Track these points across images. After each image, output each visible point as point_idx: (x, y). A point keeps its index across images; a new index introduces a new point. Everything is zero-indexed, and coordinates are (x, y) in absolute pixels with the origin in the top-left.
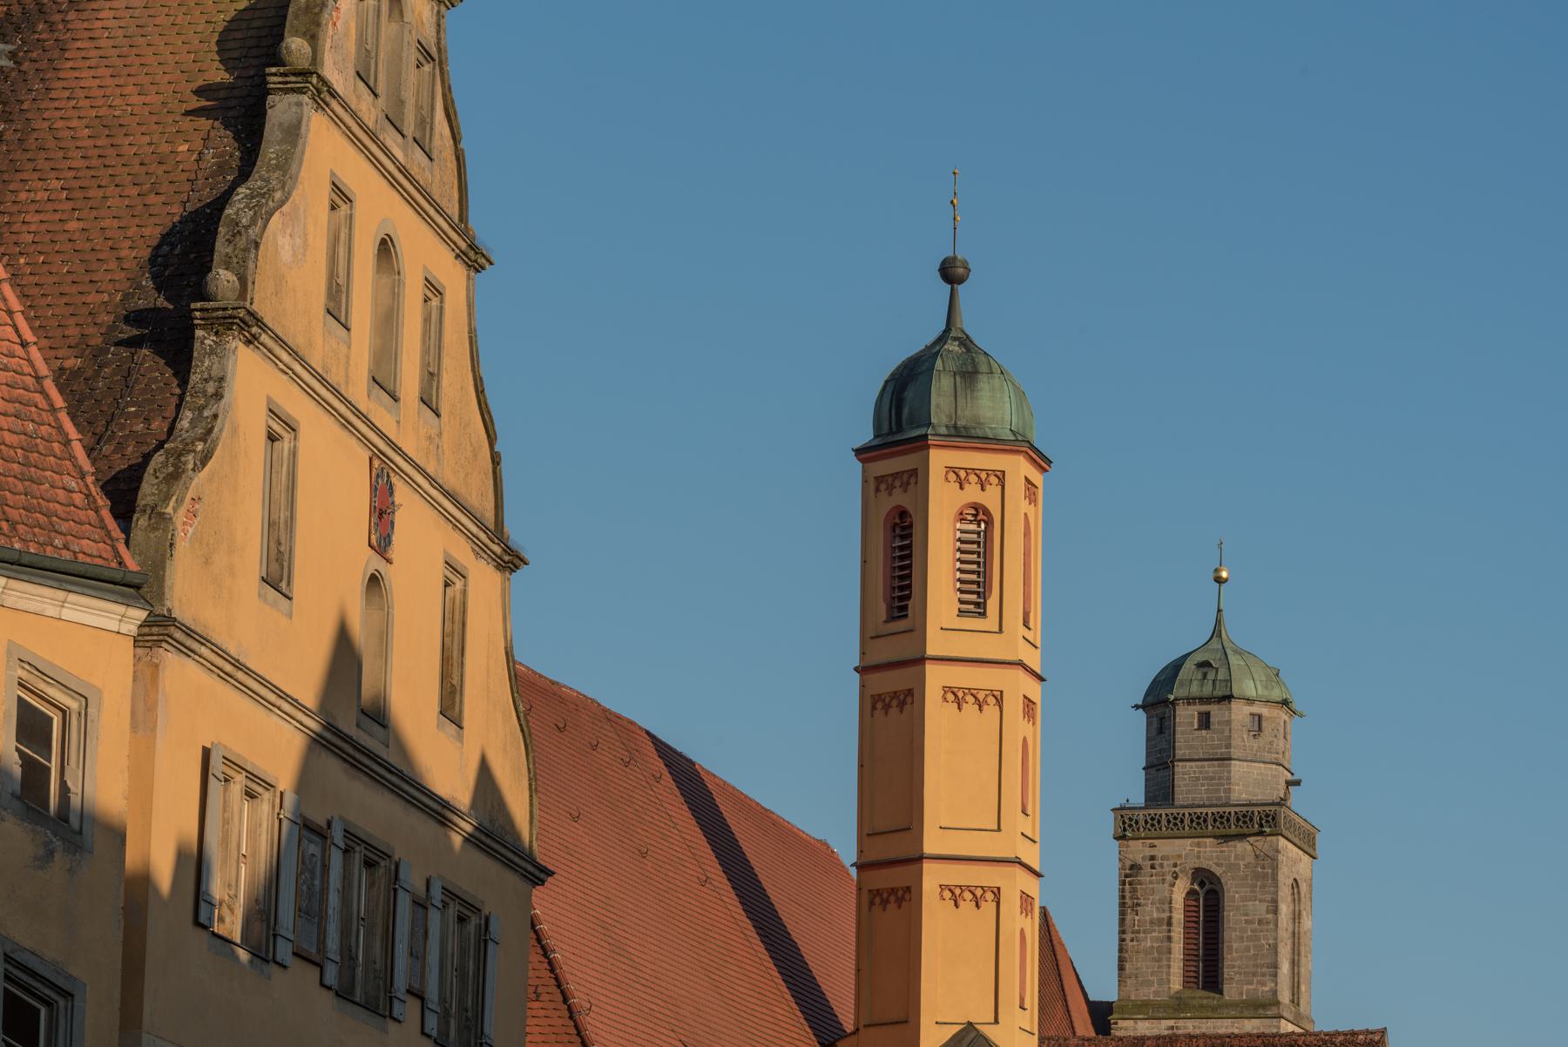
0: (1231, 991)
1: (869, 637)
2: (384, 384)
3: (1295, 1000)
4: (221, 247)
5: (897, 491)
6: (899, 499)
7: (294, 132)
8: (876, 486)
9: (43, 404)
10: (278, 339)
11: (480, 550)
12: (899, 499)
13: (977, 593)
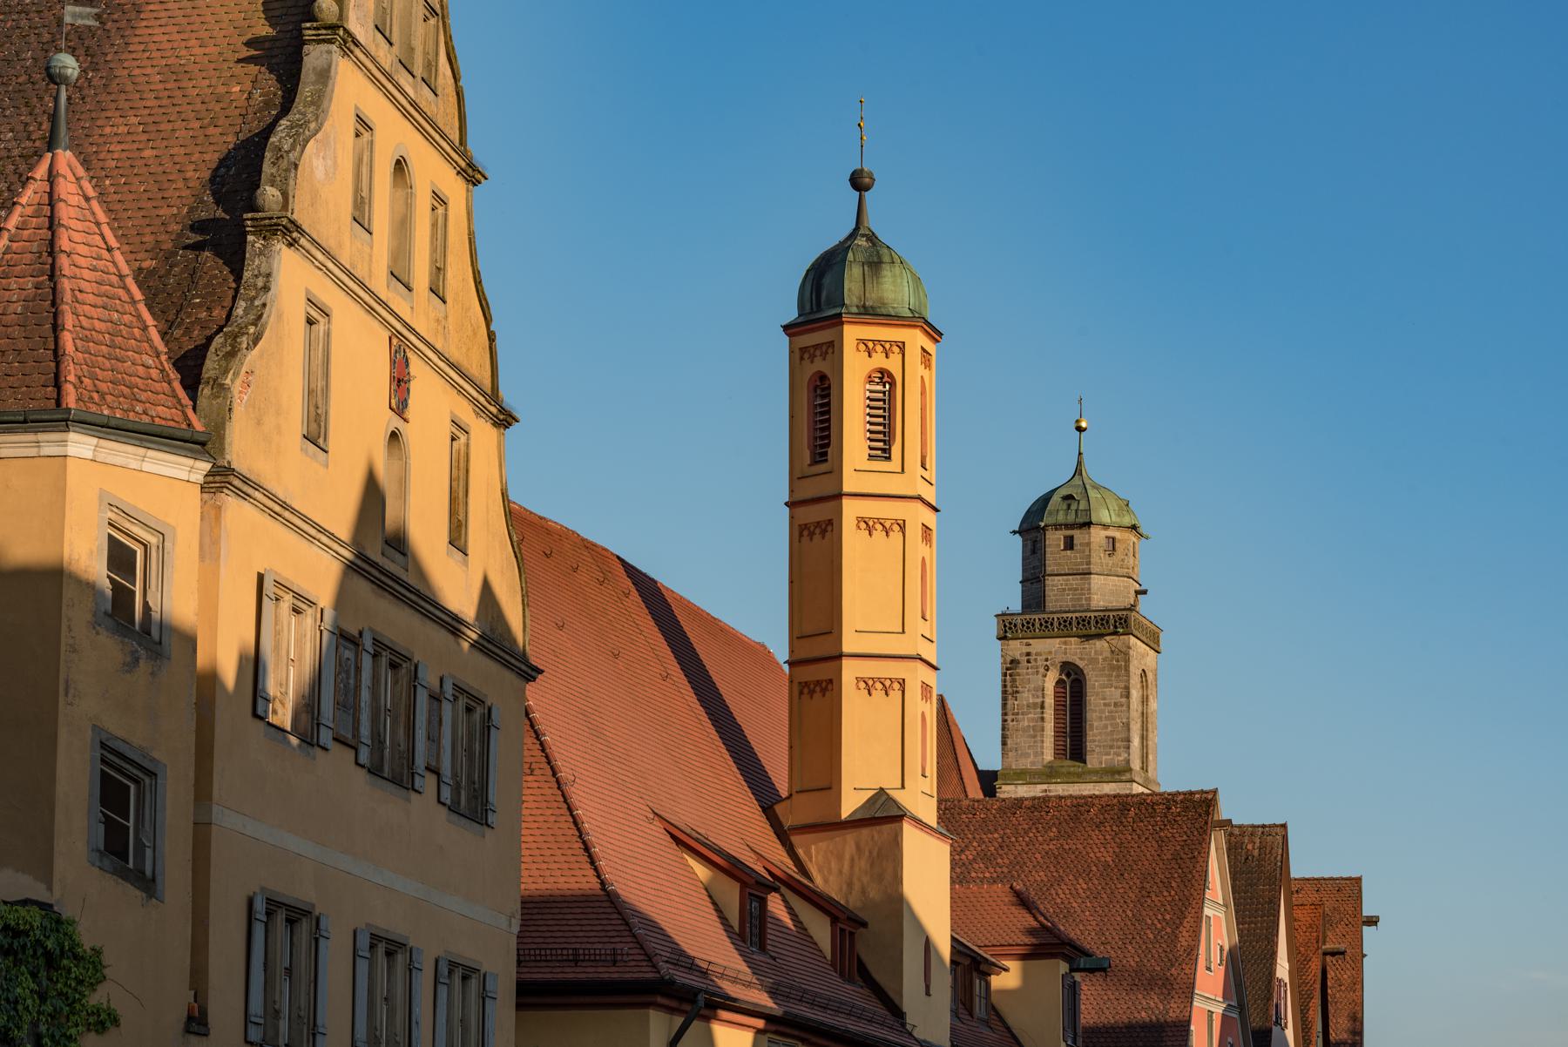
0: (1093, 761)
1: (796, 478)
2: (399, 277)
3: (1144, 768)
4: (267, 169)
5: (818, 360)
6: (820, 365)
7: (325, 75)
8: (799, 356)
9: (125, 297)
10: (313, 241)
11: (480, 410)
12: (820, 365)
13: (883, 442)
